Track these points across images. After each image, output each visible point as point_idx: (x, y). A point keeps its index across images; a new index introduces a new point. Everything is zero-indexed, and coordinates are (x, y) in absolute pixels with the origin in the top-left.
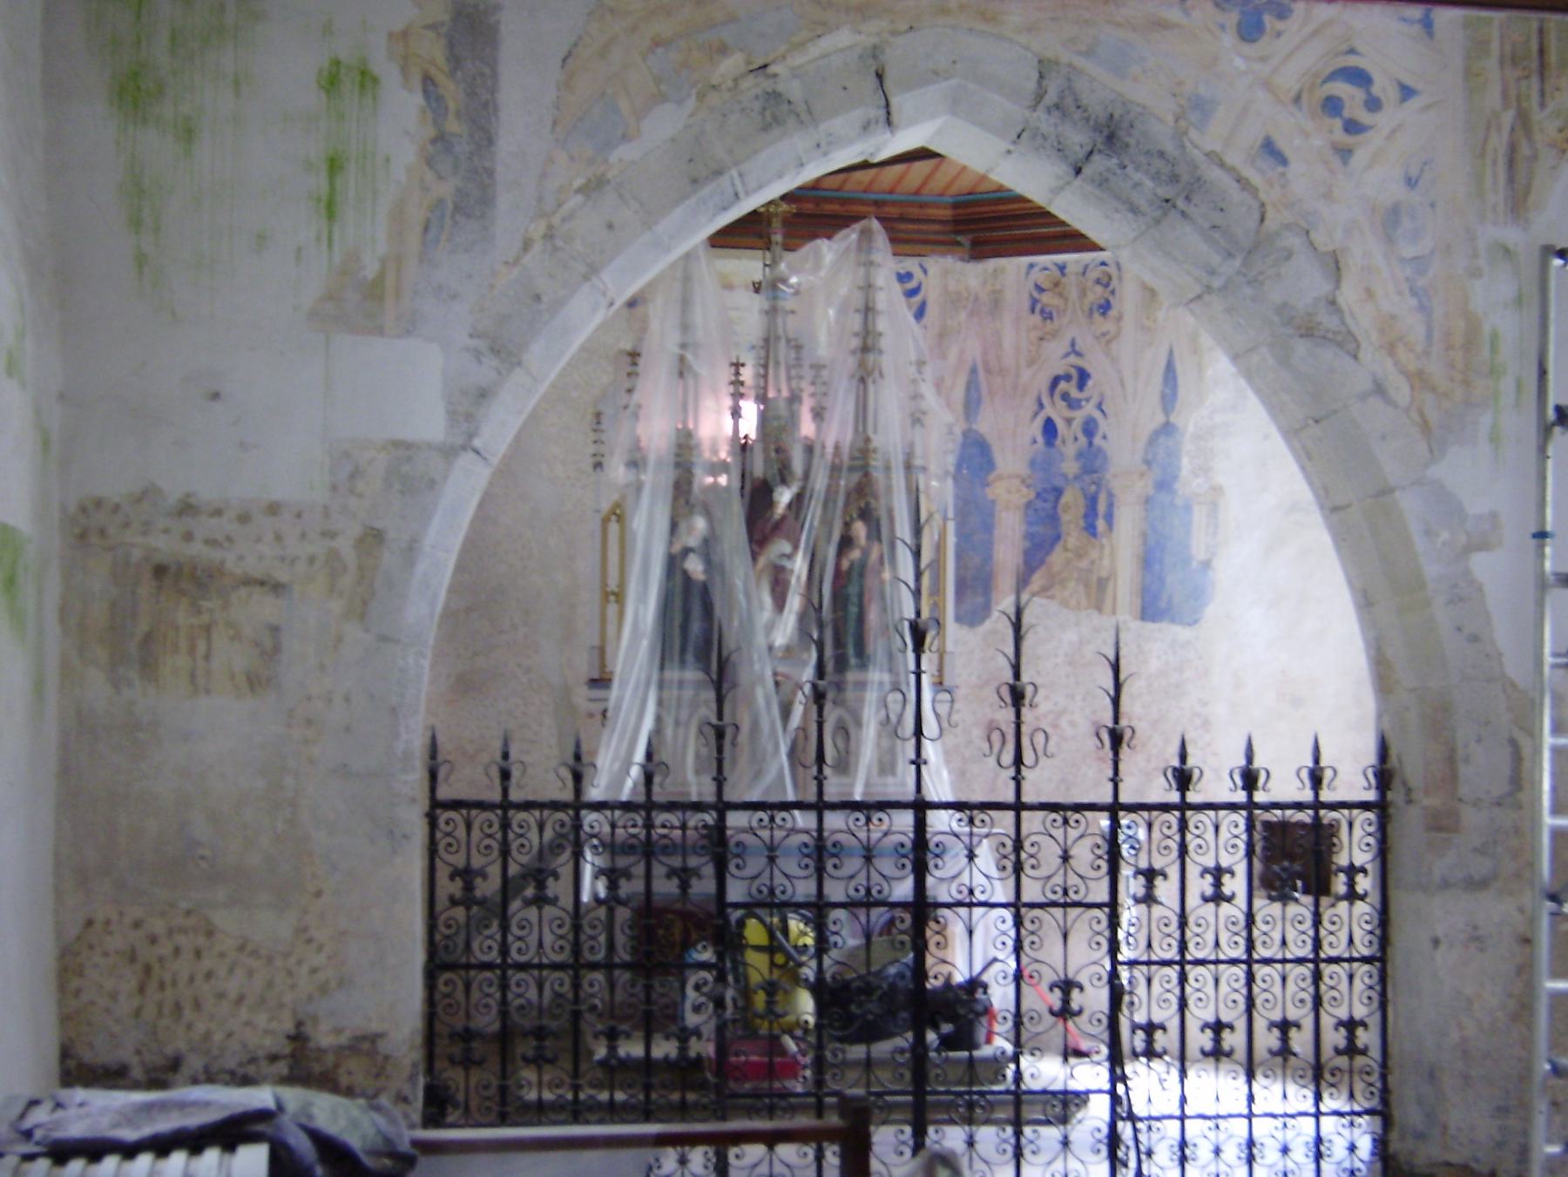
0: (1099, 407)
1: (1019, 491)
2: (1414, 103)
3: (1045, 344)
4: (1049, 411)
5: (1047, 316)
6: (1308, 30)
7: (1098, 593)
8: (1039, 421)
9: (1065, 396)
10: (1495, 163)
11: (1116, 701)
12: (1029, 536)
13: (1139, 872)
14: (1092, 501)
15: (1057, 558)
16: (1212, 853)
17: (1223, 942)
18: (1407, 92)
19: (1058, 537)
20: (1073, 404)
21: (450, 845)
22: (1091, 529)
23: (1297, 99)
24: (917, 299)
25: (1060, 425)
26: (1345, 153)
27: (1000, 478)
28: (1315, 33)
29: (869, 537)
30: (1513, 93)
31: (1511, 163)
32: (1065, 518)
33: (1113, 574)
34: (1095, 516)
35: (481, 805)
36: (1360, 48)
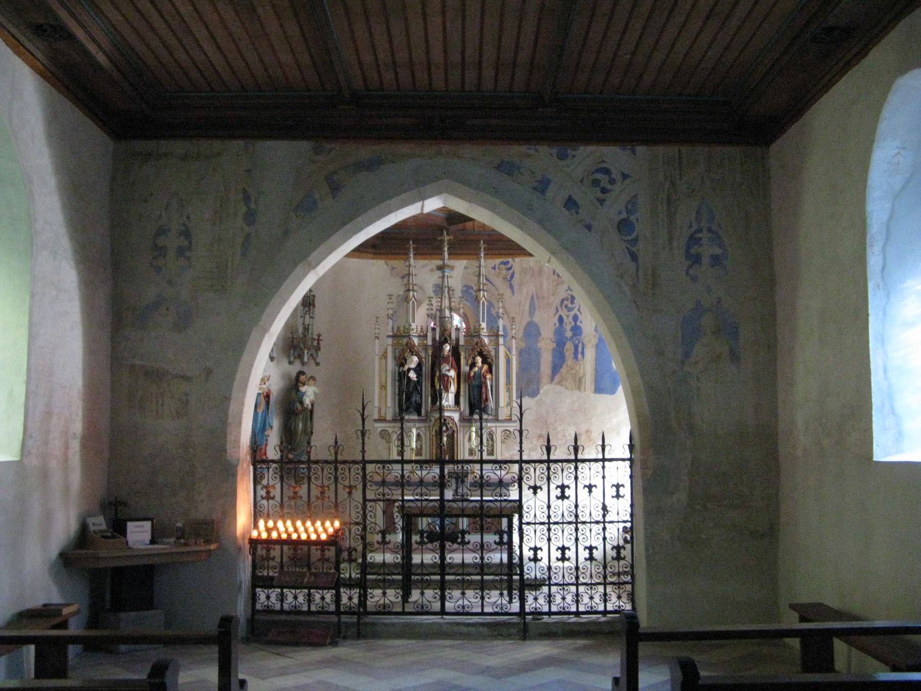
0: (579, 310)
1: (549, 344)
2: (628, 181)
3: (558, 286)
4: (560, 312)
7: (579, 383)
9: (566, 307)
12: (553, 362)
13: (530, 487)
14: (576, 347)
15: (564, 370)
18: (625, 176)
19: (564, 362)
20: (570, 310)
21: (343, 478)
23: (582, 181)
24: (511, 272)
25: (564, 317)
26: (601, 201)
27: (543, 339)
29: (483, 363)
32: (567, 354)
33: (584, 375)
34: (578, 352)
35: (326, 462)
36: (605, 159)
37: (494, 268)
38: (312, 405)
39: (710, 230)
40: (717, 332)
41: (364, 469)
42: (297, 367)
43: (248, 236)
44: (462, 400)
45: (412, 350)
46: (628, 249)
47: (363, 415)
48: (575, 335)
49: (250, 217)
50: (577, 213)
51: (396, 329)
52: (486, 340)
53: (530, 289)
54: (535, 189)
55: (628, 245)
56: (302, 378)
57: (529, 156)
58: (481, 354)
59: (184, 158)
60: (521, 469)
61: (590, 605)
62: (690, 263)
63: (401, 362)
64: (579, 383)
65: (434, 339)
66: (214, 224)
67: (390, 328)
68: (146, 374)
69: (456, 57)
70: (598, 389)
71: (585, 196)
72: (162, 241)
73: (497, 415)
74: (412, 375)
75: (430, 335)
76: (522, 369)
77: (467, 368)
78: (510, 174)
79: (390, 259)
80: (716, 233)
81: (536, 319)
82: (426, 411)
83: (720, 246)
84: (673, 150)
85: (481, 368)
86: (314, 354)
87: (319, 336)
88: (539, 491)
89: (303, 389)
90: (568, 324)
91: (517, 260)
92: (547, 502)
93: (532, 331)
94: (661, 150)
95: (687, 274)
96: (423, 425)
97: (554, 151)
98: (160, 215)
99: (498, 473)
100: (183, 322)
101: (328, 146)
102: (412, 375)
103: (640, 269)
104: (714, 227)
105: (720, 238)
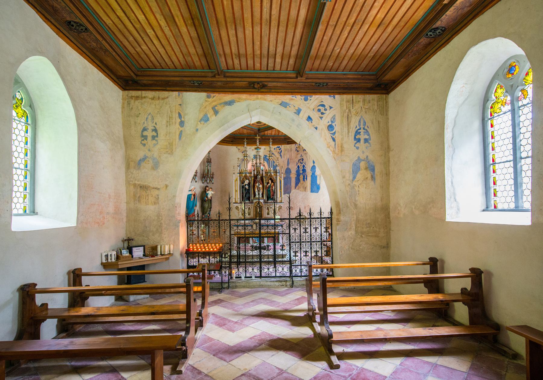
2: (332, 109)
4: (298, 164)
5: (298, 151)
6: (315, 99)
8: (297, 166)
9: (300, 162)
10: (345, 118)
11: (289, 203)
14: (304, 176)
15: (300, 184)
16: (294, 226)
17: (317, 238)
18: (331, 108)
19: (300, 181)
20: (302, 163)
22: (304, 180)
26: (321, 118)
28: (316, 99)
29: (271, 182)
30: (348, 107)
31: (348, 118)
32: (301, 179)
34: (305, 178)
35: (215, 220)
37: (275, 149)
38: (211, 198)
39: (364, 129)
40: (366, 169)
41: (230, 223)
42: (205, 184)
43: (181, 131)
44: (264, 195)
45: (246, 177)
46: (331, 136)
47: (229, 202)
48: (303, 172)
49: (182, 124)
50: (312, 122)
51: (240, 170)
52: (273, 174)
53: (287, 156)
54: (295, 113)
55: (332, 135)
56: (207, 188)
57: (292, 99)
58: (271, 179)
59: (153, 99)
60: (290, 222)
61: (316, 273)
62: (356, 141)
63: (243, 182)
64: (305, 189)
65: (254, 174)
66: (167, 126)
67: (239, 170)
68: (141, 187)
69: (265, 52)
70: (312, 191)
71: (315, 116)
72: (145, 133)
73: (277, 201)
74: (247, 187)
75: (253, 172)
76: (285, 184)
77: (266, 184)
78: (286, 107)
79: (238, 146)
80: (366, 130)
81: (290, 167)
82: (252, 199)
83: (369, 135)
84: (349, 97)
85: (271, 184)
86: (211, 179)
87: (213, 173)
88: (296, 230)
89: (207, 192)
90: (301, 168)
91: (283, 146)
92: (299, 234)
93: (288, 171)
94: (345, 97)
95: (355, 146)
96: (250, 204)
97: (303, 98)
98: (144, 122)
99: (281, 223)
100: (155, 166)
101: (212, 95)
102: (247, 187)
103: (336, 145)
104: (366, 128)
105: (368, 132)
